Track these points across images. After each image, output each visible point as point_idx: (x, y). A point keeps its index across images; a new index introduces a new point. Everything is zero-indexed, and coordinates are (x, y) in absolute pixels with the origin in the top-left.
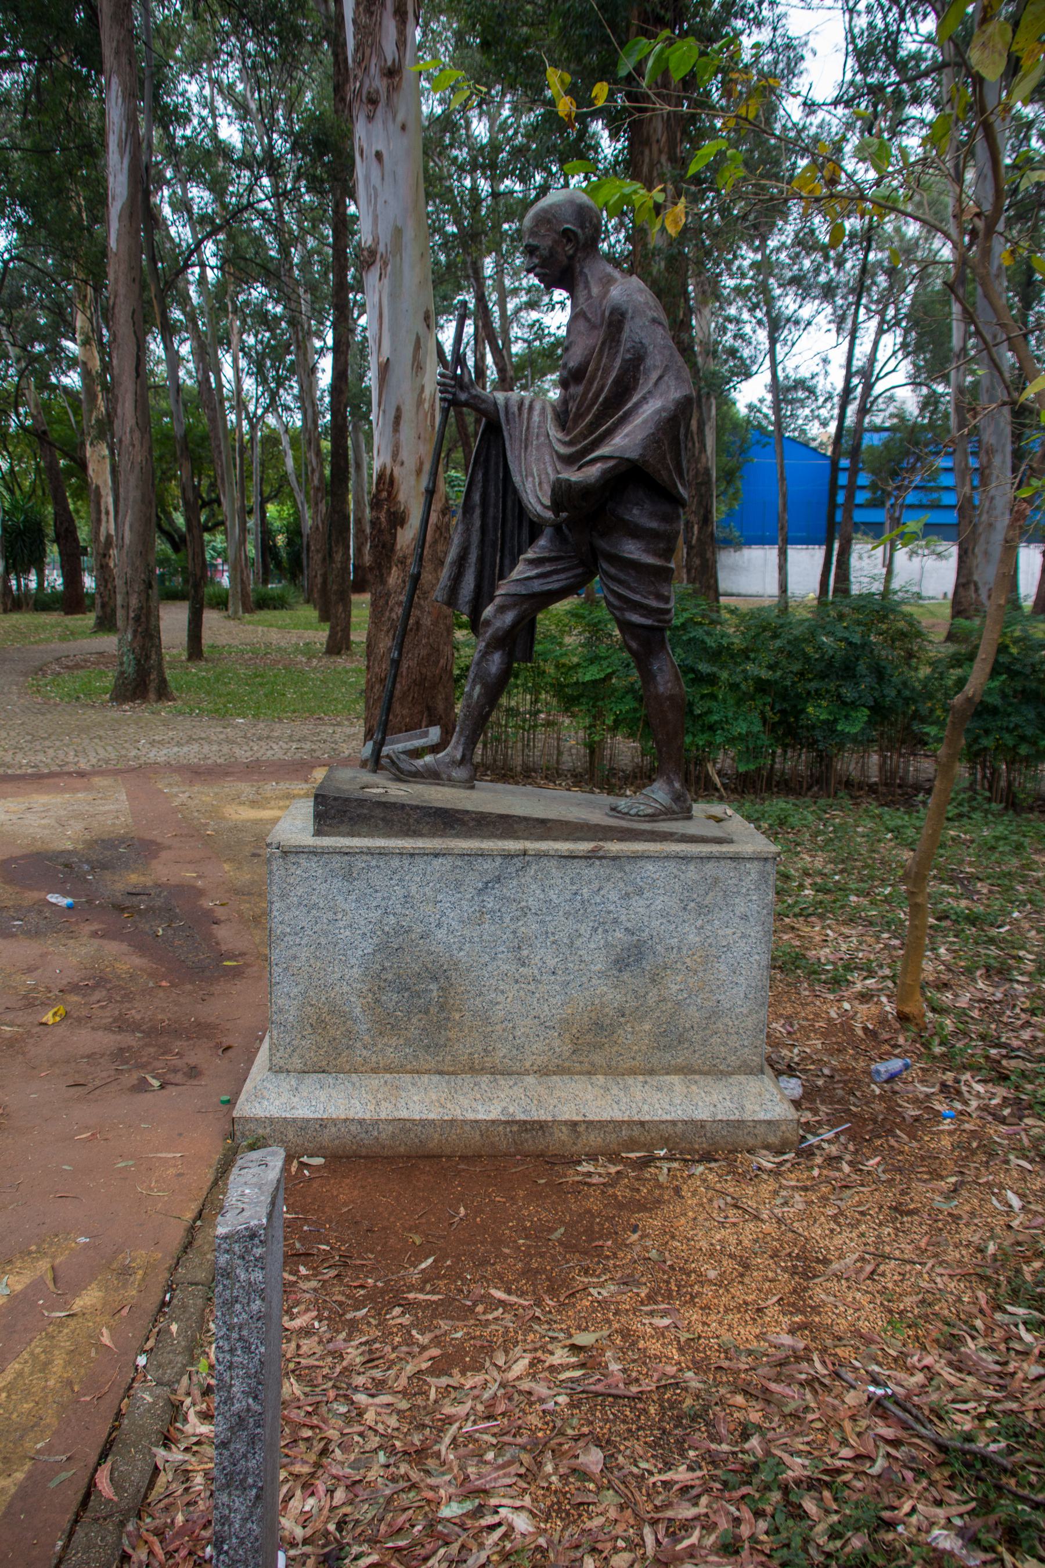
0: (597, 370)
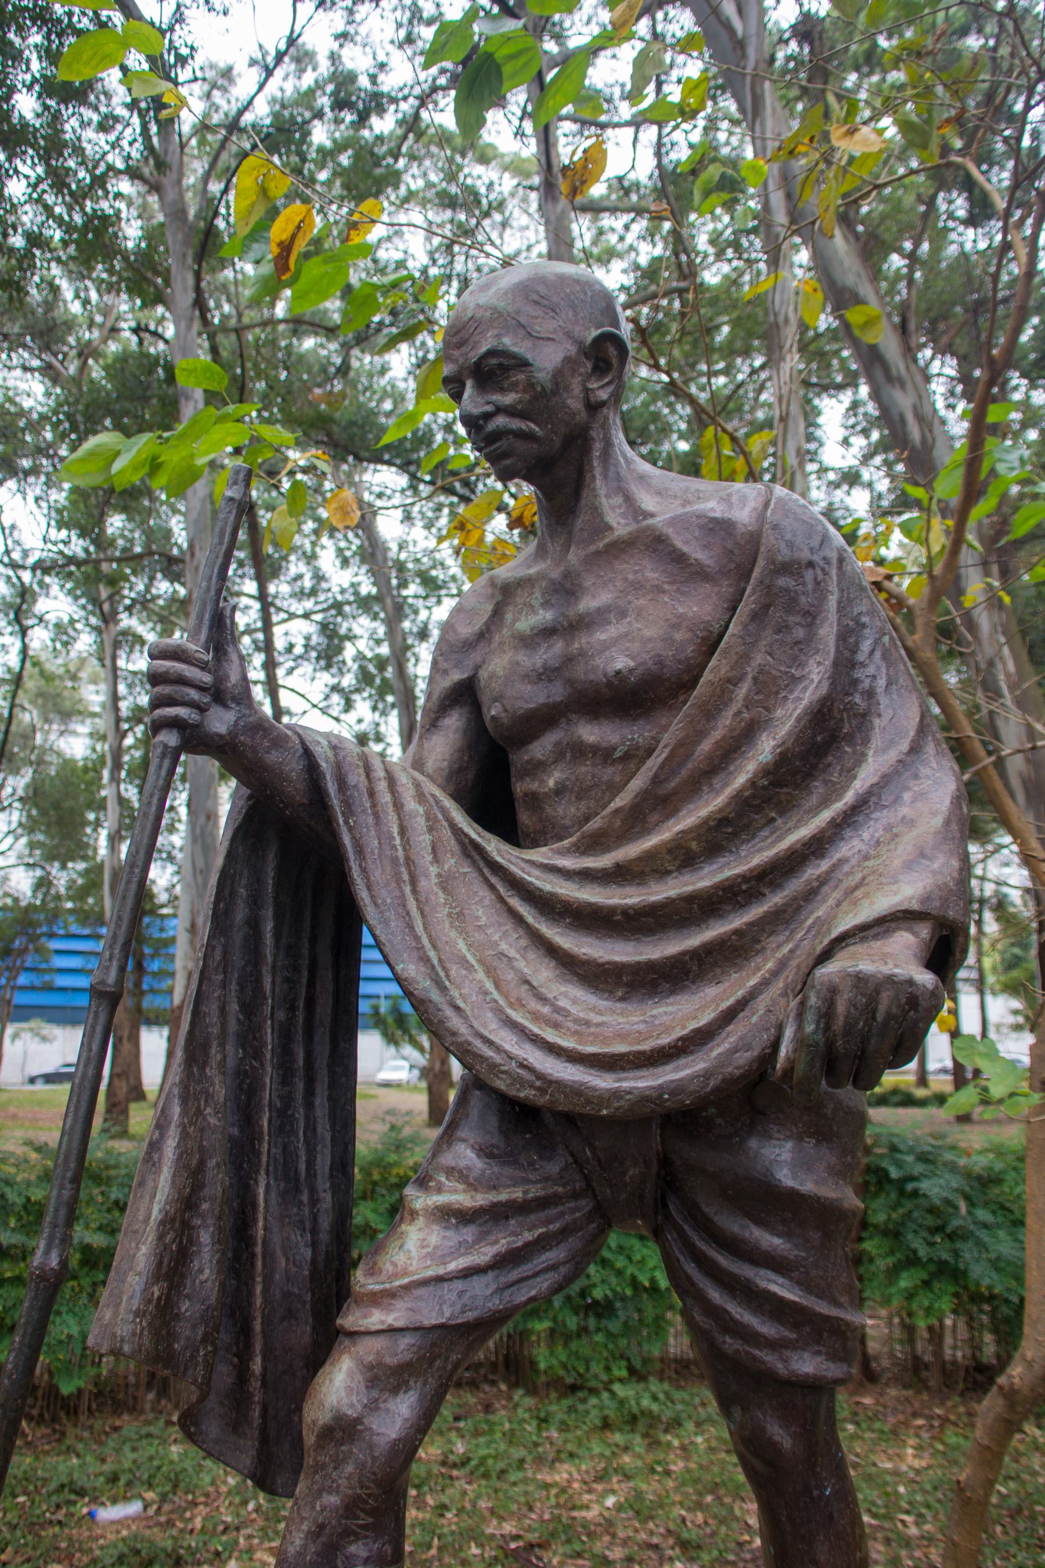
0: (734, 681)
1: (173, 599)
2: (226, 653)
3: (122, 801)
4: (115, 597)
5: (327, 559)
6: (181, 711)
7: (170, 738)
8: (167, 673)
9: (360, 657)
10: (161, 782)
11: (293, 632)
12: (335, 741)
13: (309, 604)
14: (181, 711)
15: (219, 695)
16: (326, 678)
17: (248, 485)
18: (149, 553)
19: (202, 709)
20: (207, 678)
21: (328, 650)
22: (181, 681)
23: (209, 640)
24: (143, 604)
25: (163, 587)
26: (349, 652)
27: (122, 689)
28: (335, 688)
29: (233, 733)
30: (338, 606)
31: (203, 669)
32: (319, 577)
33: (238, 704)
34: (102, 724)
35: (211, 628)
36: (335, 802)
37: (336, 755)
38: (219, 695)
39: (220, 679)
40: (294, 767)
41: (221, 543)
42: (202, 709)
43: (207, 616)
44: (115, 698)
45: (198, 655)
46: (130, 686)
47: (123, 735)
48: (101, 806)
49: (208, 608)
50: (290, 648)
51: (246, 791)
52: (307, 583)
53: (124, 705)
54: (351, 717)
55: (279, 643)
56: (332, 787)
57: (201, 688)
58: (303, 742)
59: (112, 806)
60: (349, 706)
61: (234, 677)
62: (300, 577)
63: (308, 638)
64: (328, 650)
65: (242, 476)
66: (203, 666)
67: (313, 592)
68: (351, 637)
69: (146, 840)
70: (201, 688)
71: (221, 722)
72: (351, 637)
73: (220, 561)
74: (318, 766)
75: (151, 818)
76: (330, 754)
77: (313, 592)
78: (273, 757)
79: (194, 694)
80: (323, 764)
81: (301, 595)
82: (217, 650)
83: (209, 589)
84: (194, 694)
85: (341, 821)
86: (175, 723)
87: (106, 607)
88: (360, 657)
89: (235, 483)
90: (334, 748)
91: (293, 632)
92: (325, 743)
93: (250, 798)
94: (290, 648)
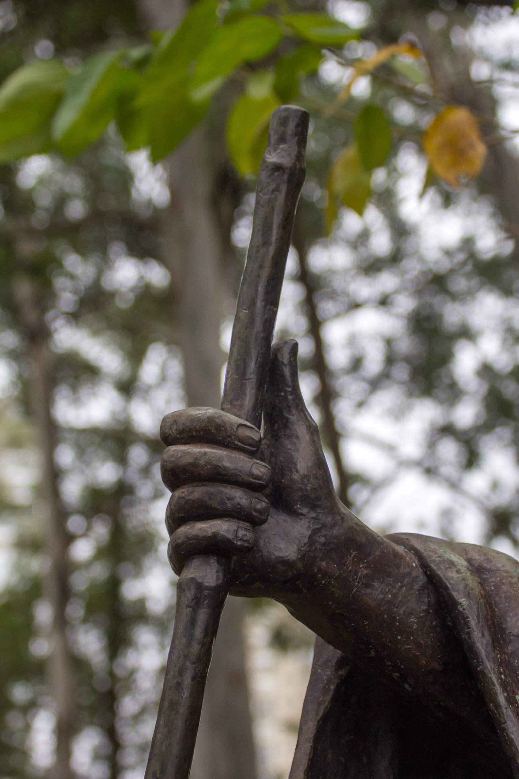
1: (145, 293)
2: (286, 424)
3: (77, 663)
4: (45, 297)
5: (414, 202)
6: (222, 527)
7: (207, 573)
8: (194, 465)
9: (486, 371)
10: (195, 648)
11: (362, 330)
12: (477, 557)
13: (387, 281)
14: (222, 527)
15: (278, 495)
16: (425, 413)
17: (302, 140)
18: (96, 216)
19: (254, 520)
20: (259, 469)
21: (425, 361)
22: (219, 476)
23: (259, 404)
24: (94, 304)
25: (126, 273)
26: (466, 362)
27: (65, 456)
28: (447, 430)
29: (307, 557)
30: (437, 283)
31: (252, 454)
32: (401, 230)
33: (313, 507)
34: (38, 522)
35: (260, 385)
36: (489, 667)
37: (482, 583)
38: (278, 495)
39: (281, 468)
40: (412, 607)
41: (266, 243)
42: (254, 520)
43: (252, 366)
44: (53, 475)
45: (242, 432)
46: (81, 452)
47: (69, 539)
48: (35, 671)
49: (254, 353)
50: (356, 364)
51: (333, 653)
52: (381, 243)
53: (72, 489)
54: (477, 482)
55: (338, 357)
56: (480, 641)
57: (251, 486)
58: (424, 565)
59: (59, 675)
60: (472, 459)
61: (303, 463)
62: (364, 236)
63: (389, 342)
64: (425, 361)
65: (291, 126)
66: (253, 450)
67: (395, 259)
68: (467, 333)
69: (175, 750)
70: (251, 486)
71: (285, 539)
72: (467, 333)
73: (266, 273)
74: (455, 603)
75: (183, 710)
76: (473, 582)
77: (395, 259)
78: (377, 593)
79: (239, 497)
80: (463, 601)
81: (372, 267)
82: (271, 420)
83: (251, 320)
84: (239, 497)
85: (501, 699)
86: (213, 548)
87: (30, 316)
88: (486, 371)
89: (282, 140)
90: (478, 570)
91: (362, 330)
92: (461, 562)
93: (341, 664)
94: (356, 364)
